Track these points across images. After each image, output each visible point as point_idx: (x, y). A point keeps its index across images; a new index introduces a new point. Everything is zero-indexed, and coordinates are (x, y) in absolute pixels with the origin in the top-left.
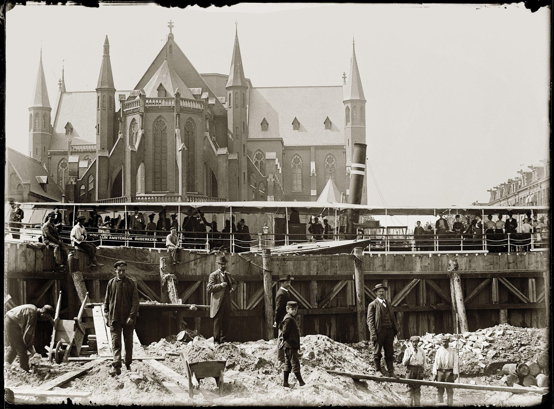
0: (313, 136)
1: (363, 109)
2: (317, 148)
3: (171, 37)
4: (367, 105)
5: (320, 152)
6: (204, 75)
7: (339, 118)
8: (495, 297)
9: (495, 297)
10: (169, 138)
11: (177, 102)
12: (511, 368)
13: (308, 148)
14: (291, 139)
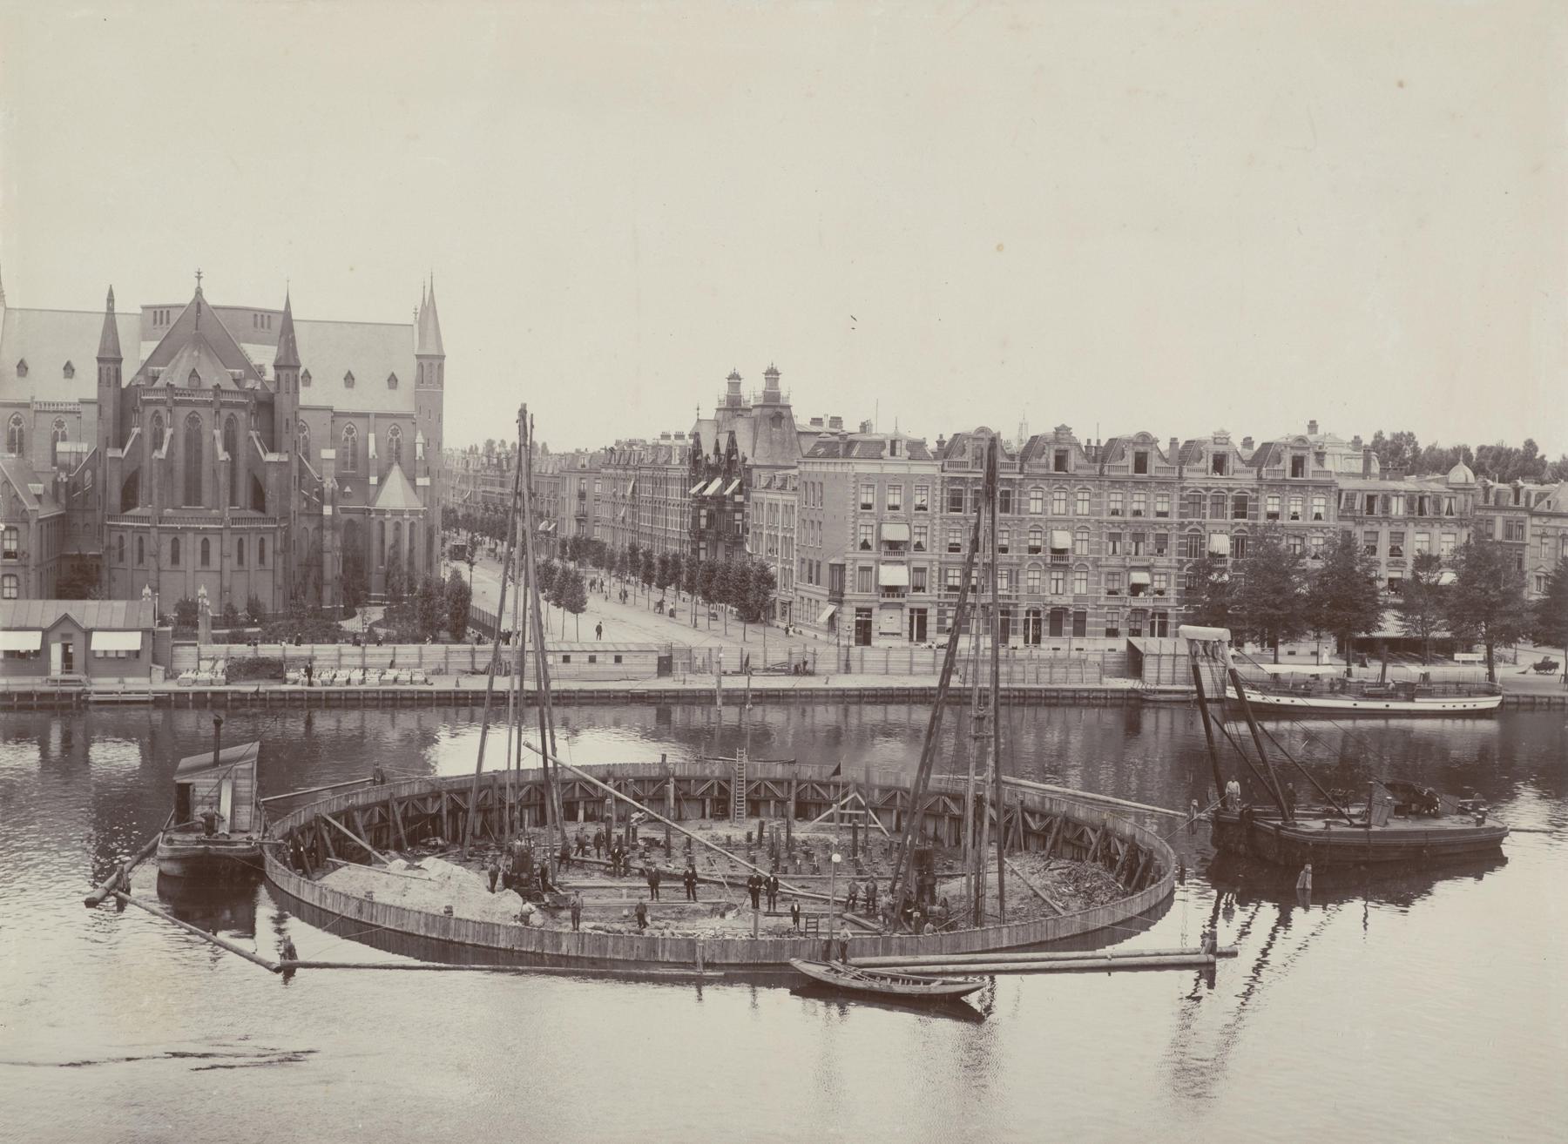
0: (371, 398)
1: (441, 367)
2: (378, 416)
3: (199, 292)
4: (447, 363)
5: (381, 421)
6: (216, 308)
7: (408, 373)
8: (577, 794)
9: (577, 794)
10: (206, 440)
11: (216, 395)
12: (115, 757)
13: (365, 415)
14: (345, 401)
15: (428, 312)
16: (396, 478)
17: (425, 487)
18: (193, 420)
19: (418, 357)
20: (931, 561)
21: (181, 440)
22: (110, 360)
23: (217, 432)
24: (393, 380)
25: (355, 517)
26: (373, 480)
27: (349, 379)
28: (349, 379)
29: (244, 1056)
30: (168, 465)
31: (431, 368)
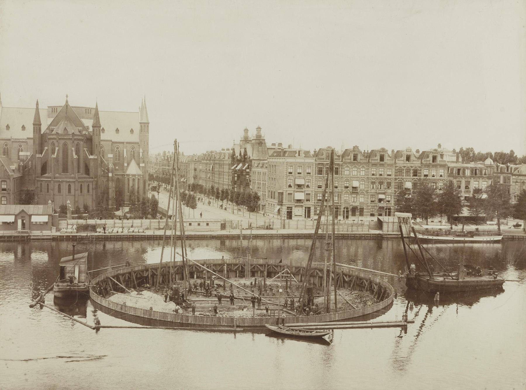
3: (67, 102)
7: (137, 128)
11: (73, 136)
16: (133, 163)
17: (143, 167)
18: (65, 145)
19: (140, 123)
23: (73, 149)
25: (120, 177)
26: (126, 165)
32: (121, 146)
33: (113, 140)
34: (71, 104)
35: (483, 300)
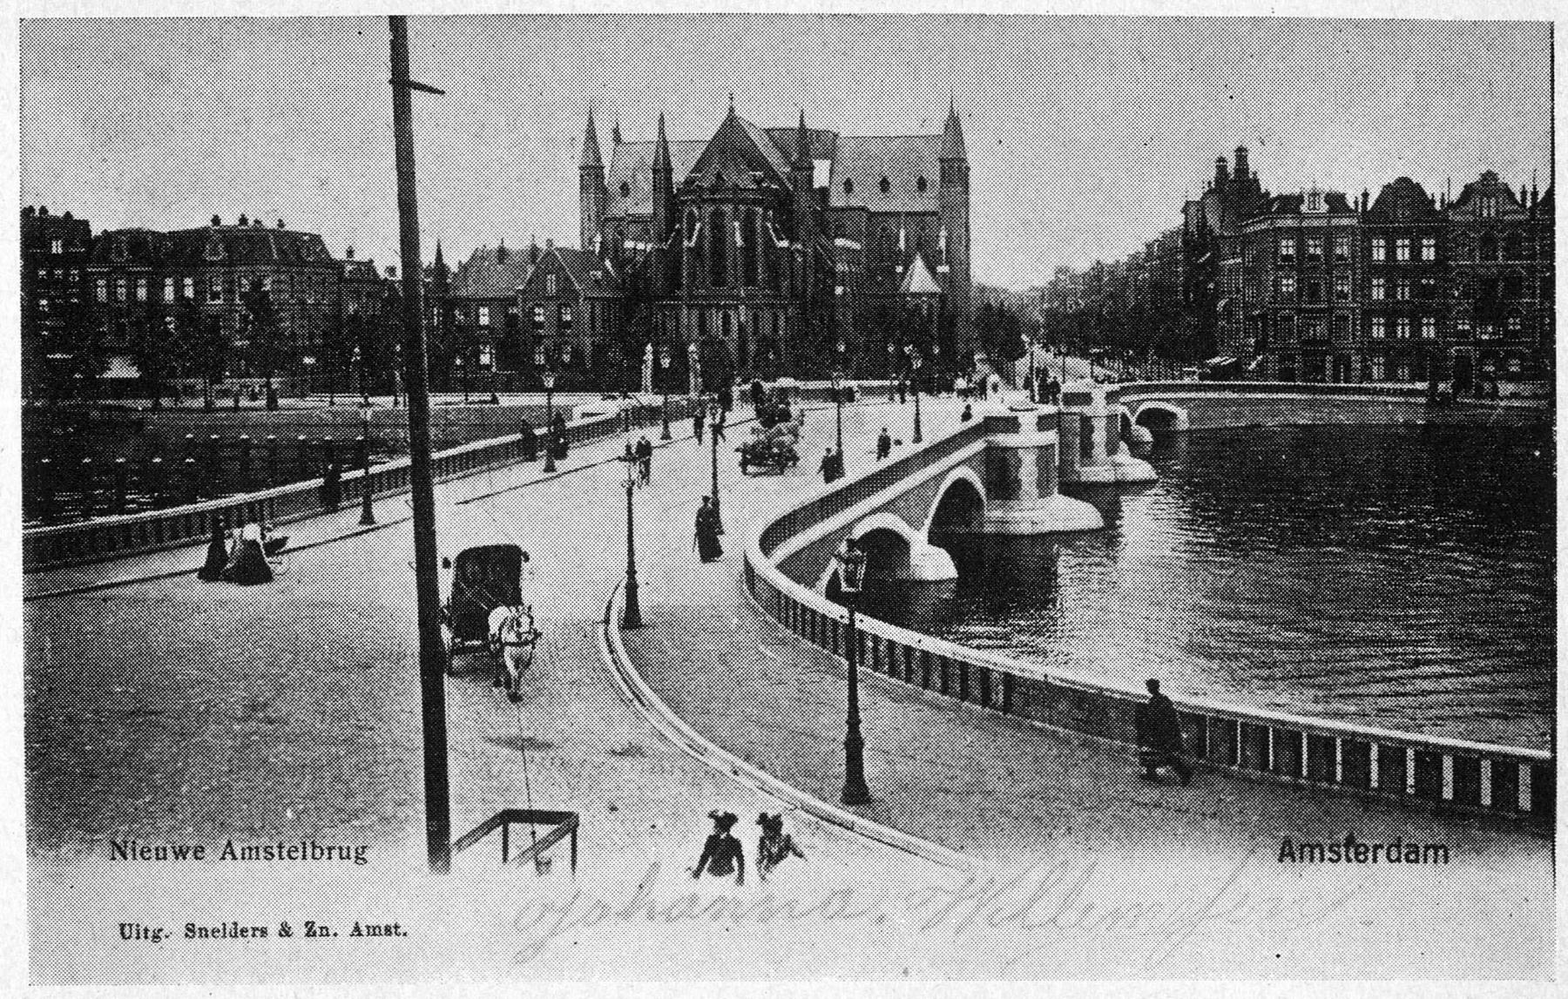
3: (732, 110)
7: (933, 174)
11: (735, 193)
15: (953, 124)
16: (919, 264)
17: (944, 274)
18: (718, 215)
19: (941, 160)
20: (1353, 309)
21: (707, 232)
22: (663, 170)
23: (737, 224)
24: (922, 184)
25: (887, 302)
26: (899, 269)
27: (885, 185)
28: (885, 185)
29: (592, 415)
30: (697, 252)
31: (955, 172)
32: (892, 221)
33: (872, 209)
34: (809, 124)
35: (943, 551)
